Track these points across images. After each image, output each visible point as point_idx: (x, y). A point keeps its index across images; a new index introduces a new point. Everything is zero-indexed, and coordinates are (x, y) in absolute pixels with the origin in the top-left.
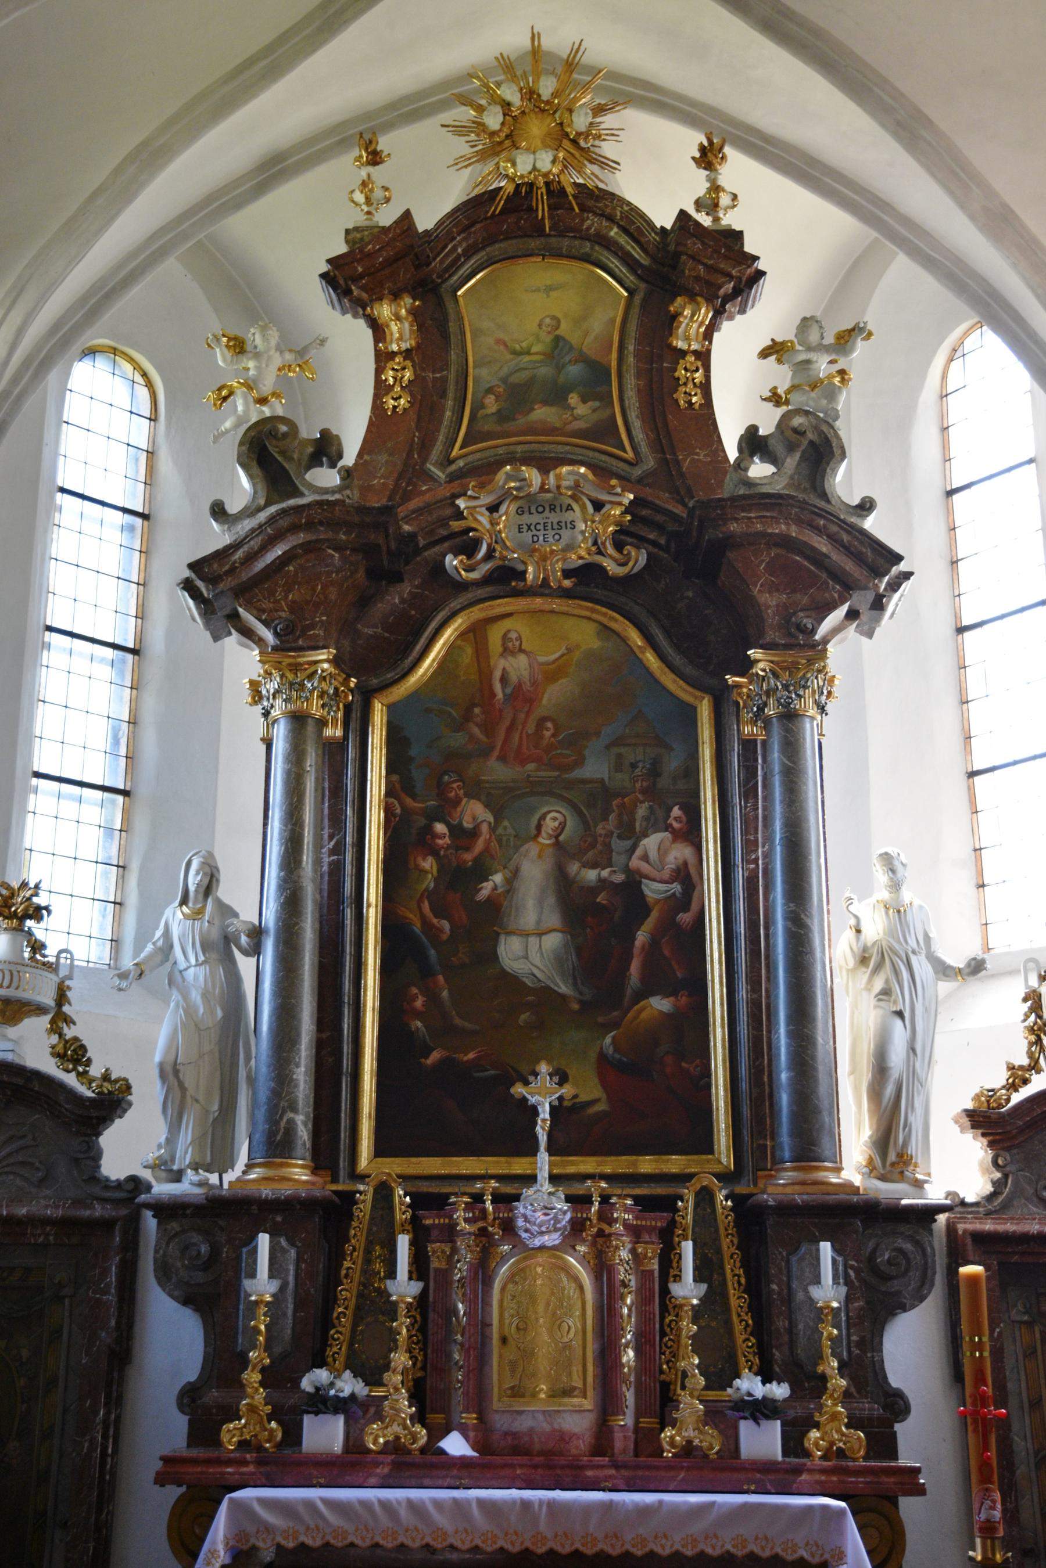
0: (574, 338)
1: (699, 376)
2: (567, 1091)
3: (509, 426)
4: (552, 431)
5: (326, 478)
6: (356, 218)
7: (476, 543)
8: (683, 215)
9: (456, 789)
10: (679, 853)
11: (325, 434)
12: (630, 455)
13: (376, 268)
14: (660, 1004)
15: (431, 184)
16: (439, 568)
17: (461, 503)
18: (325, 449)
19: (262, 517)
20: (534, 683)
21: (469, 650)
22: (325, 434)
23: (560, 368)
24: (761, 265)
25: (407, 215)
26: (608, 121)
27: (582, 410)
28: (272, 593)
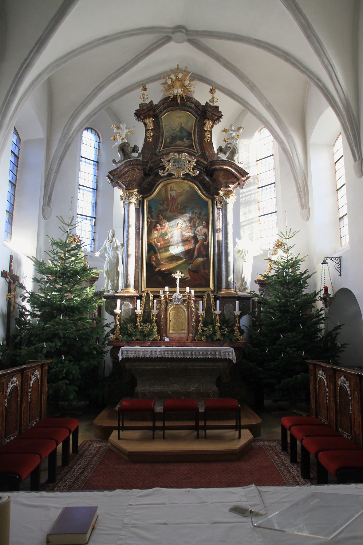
0: (185, 127)
1: (209, 136)
2: (183, 275)
3: (172, 145)
4: (180, 146)
5: (135, 155)
6: (141, 102)
7: (165, 168)
8: (207, 103)
9: (161, 217)
10: (205, 230)
11: (135, 146)
12: (196, 151)
13: (145, 112)
14: (200, 259)
15: (155, 95)
16: (158, 174)
17: (162, 160)
18: (135, 149)
19: (123, 162)
20: (177, 197)
21: (164, 190)
22: (135, 146)
23: (182, 133)
24: (222, 114)
25: (152, 101)
26: (192, 83)
27: (186, 142)
28: (125, 178)
